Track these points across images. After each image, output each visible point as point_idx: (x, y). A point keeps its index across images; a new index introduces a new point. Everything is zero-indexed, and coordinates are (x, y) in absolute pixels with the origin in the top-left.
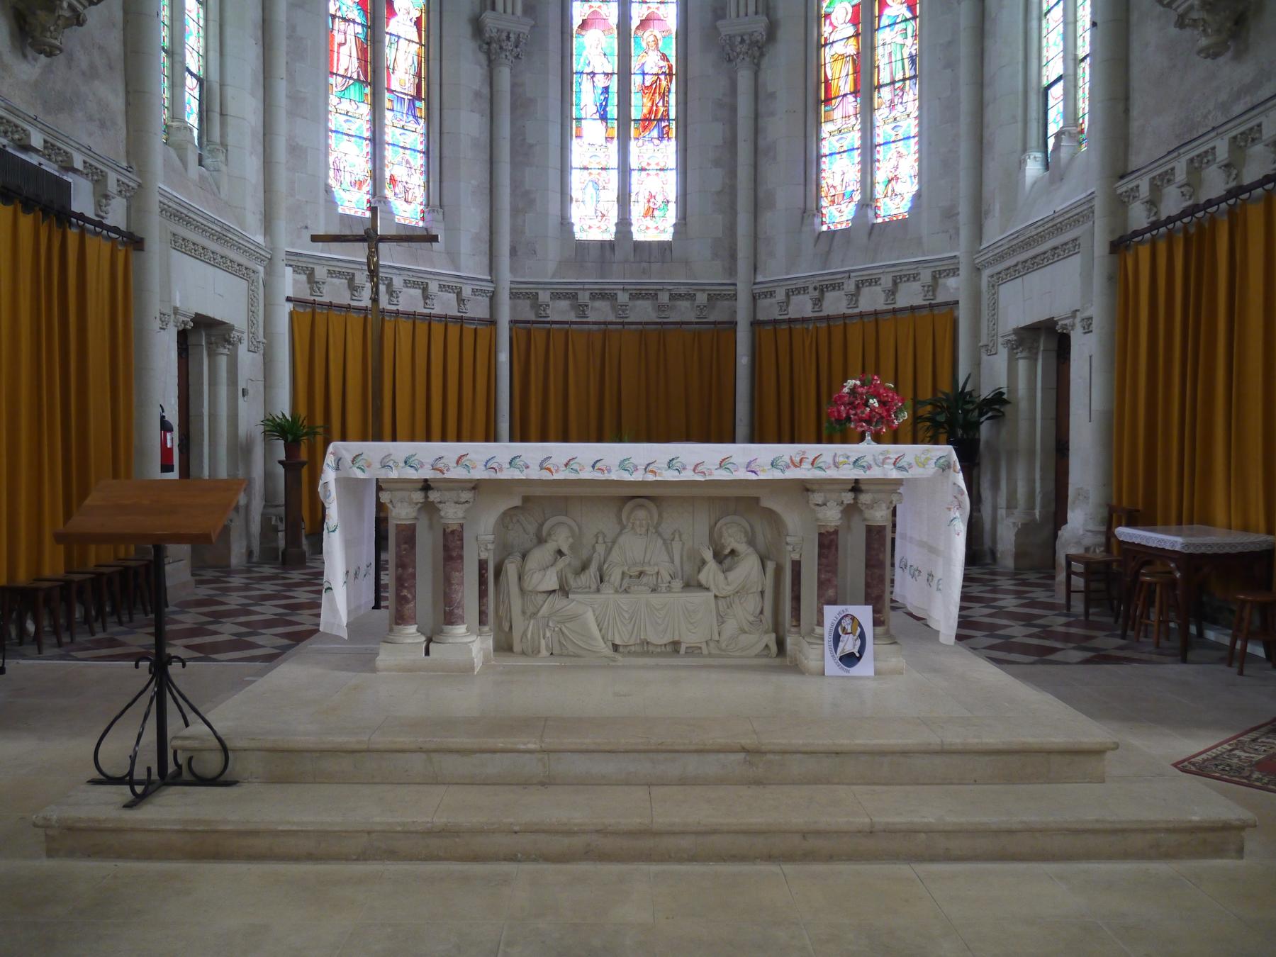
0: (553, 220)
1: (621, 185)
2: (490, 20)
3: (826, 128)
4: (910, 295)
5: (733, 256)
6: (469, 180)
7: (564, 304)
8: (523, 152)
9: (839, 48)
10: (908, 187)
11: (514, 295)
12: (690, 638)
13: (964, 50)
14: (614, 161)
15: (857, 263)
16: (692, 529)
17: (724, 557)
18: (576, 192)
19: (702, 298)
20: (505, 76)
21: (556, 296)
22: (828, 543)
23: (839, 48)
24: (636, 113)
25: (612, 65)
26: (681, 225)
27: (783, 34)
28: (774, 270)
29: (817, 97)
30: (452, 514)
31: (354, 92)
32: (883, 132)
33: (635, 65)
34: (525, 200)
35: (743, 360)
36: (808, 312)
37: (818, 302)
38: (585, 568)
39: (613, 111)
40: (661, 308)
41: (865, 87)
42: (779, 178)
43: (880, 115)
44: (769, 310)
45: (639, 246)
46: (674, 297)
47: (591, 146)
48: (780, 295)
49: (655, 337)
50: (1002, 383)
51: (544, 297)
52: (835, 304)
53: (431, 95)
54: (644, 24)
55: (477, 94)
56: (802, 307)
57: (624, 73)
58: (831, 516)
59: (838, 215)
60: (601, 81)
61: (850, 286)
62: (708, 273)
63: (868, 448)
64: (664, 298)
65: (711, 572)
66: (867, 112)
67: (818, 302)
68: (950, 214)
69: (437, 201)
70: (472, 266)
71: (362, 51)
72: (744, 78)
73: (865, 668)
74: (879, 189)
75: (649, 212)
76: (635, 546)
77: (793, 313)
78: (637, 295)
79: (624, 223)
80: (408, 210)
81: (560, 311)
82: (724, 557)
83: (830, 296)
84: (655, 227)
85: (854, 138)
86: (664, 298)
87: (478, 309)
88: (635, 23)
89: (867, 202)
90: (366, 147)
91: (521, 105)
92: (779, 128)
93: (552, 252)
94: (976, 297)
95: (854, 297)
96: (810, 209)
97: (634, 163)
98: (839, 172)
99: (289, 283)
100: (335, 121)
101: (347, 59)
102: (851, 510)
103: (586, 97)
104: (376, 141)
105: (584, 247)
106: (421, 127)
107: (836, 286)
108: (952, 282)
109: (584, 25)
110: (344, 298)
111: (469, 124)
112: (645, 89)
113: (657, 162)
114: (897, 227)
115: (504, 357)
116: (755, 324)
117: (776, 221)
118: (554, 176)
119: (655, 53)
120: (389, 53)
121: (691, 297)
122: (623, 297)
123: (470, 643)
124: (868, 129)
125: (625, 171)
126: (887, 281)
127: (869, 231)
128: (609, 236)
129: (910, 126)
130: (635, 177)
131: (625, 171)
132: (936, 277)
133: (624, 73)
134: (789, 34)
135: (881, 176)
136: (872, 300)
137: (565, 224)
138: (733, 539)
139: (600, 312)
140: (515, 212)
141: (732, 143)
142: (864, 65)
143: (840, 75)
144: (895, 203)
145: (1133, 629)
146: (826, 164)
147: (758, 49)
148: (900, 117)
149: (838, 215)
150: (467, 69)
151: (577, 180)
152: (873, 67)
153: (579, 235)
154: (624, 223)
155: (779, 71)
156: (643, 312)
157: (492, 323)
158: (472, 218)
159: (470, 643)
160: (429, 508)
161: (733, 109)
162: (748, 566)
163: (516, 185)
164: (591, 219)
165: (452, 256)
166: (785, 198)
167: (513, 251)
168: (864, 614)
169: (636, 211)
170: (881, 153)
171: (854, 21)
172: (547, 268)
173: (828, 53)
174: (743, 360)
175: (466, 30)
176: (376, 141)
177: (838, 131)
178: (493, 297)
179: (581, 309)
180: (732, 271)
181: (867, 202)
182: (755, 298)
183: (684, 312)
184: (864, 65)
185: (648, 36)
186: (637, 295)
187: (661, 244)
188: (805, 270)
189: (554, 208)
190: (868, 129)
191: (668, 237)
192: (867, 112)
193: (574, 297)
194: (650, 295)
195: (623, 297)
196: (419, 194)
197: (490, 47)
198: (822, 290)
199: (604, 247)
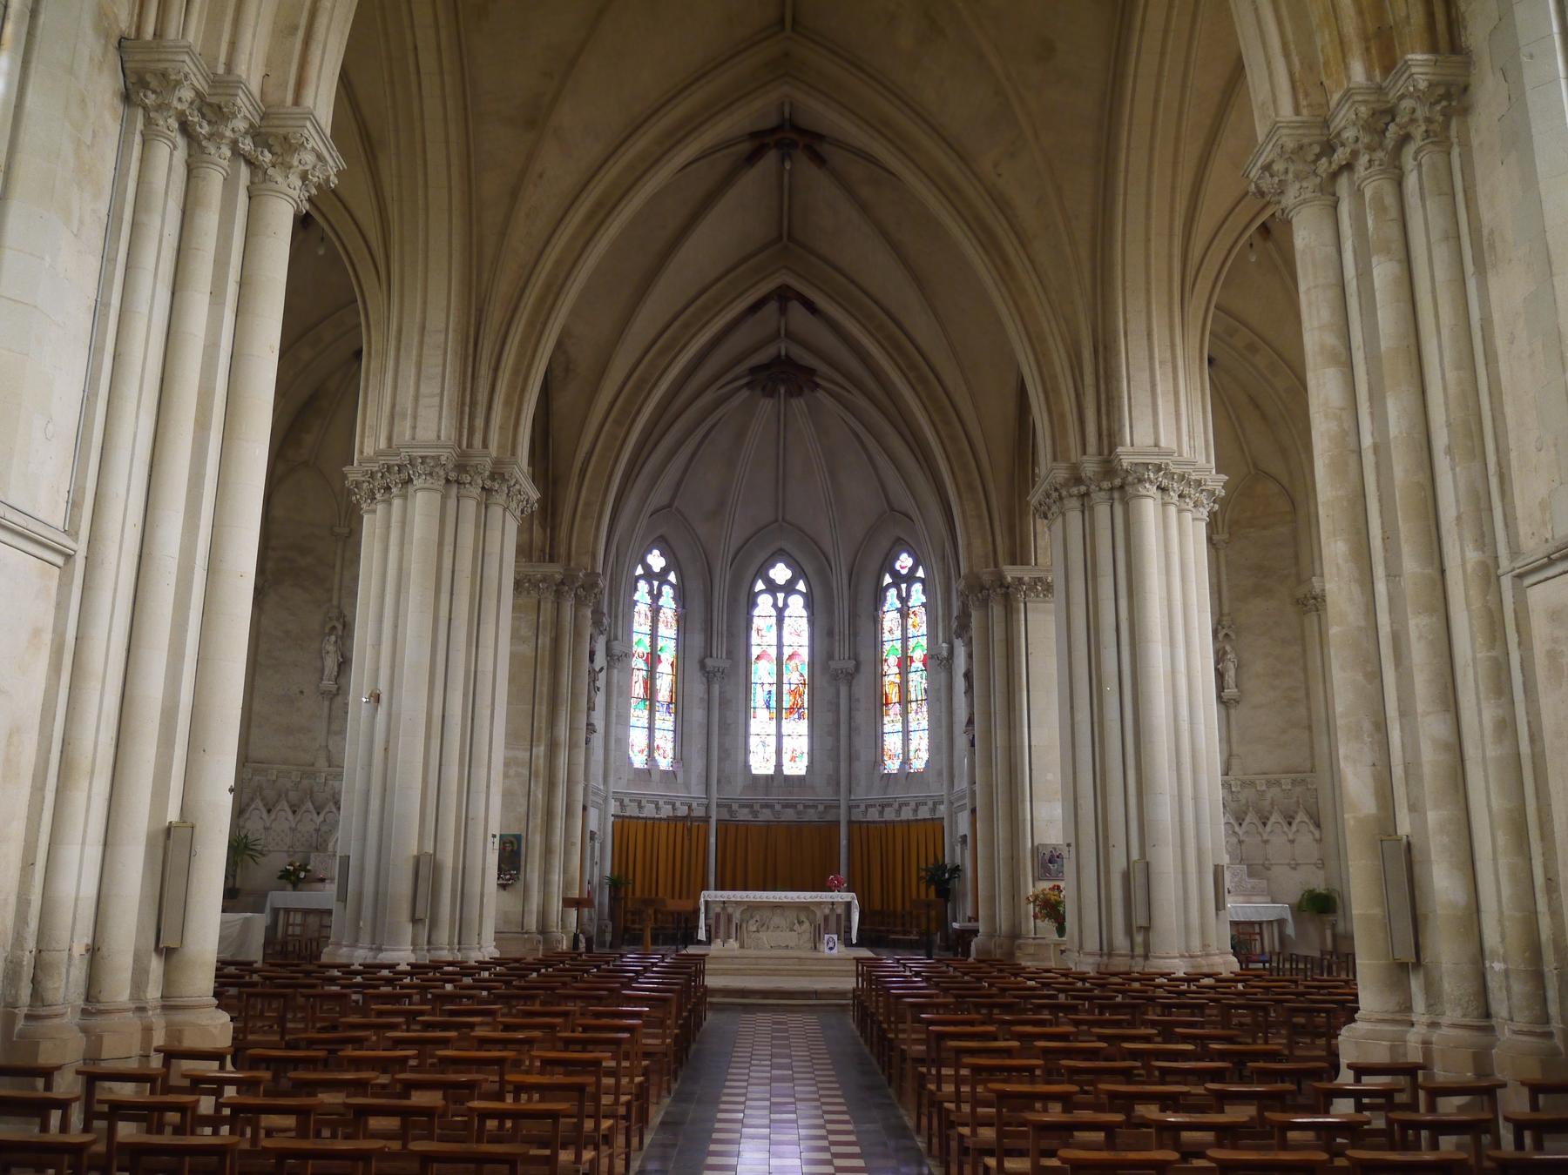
0: (741, 764)
1: (778, 744)
2: (709, 662)
3: (886, 719)
4: (924, 813)
5: (838, 784)
6: (697, 744)
7: (746, 810)
8: (725, 728)
9: (891, 678)
10: (925, 756)
11: (718, 806)
12: (791, 944)
13: (943, 694)
14: (774, 731)
15: (897, 793)
16: (792, 915)
17: (801, 923)
18: (752, 747)
19: (821, 808)
20: (716, 689)
21: (741, 806)
22: (826, 918)
23: (891, 678)
24: (785, 705)
25: (774, 679)
26: (810, 768)
27: (863, 669)
28: (860, 794)
29: (881, 703)
30: (730, 910)
31: (641, 705)
32: (913, 726)
33: (785, 680)
34: (725, 753)
35: (844, 842)
36: (877, 818)
37: (881, 813)
38: (763, 925)
39: (773, 704)
40: (799, 813)
41: (904, 701)
42: (861, 743)
43: (912, 716)
44: (857, 815)
45: (787, 777)
46: (806, 807)
47: (761, 724)
48: (863, 808)
49: (796, 830)
50: (958, 861)
51: (735, 807)
52: (890, 815)
53: (678, 702)
54: (791, 657)
55: (702, 699)
56: (873, 815)
57: (780, 684)
58: (827, 911)
59: (892, 766)
60: (767, 688)
61: (896, 806)
62: (824, 793)
63: (836, 893)
64: (800, 807)
65: (797, 927)
66: (905, 714)
67: (881, 813)
68: (940, 774)
69: (680, 756)
70: (697, 791)
71: (645, 683)
72: (844, 690)
73: (835, 951)
74: (912, 754)
75: (793, 759)
76: (777, 920)
77: (869, 818)
78: (785, 806)
79: (779, 765)
80: (664, 763)
81: (743, 815)
82: (801, 923)
83: (887, 810)
84: (796, 767)
85: (899, 727)
86: (800, 807)
87: (699, 812)
88: (785, 657)
89: (906, 761)
90: (646, 732)
91: (724, 703)
92: (861, 717)
93: (740, 782)
94: (951, 816)
95: (898, 811)
96: (878, 761)
97: (785, 731)
98: (893, 742)
99: (613, 807)
100: (633, 721)
101: (638, 689)
102: (832, 910)
103: (759, 696)
104: (651, 728)
105: (757, 778)
106: (672, 718)
107: (890, 805)
108: (942, 808)
109: (758, 658)
110: (636, 813)
111: (697, 715)
112: (791, 692)
113: (798, 733)
114: (918, 775)
115: (713, 840)
116: (850, 823)
117: (861, 767)
118: (741, 740)
119: (797, 673)
120: (658, 682)
121: (815, 807)
122: (778, 807)
123: (733, 944)
124: (905, 722)
125: (779, 736)
126: (913, 805)
127: (906, 776)
128: (771, 771)
129: (925, 724)
130: (785, 740)
131: (779, 736)
132: (935, 804)
133: (780, 684)
134: (866, 669)
135: (912, 748)
136: (907, 814)
137: (747, 766)
138: (803, 918)
139: (766, 815)
140: (720, 760)
141: (837, 724)
142: (903, 687)
143: (893, 693)
144: (919, 763)
145: (839, 916)
146: (887, 737)
147: (850, 676)
148: (920, 720)
149: (892, 766)
150: (697, 688)
151: (754, 742)
152: (908, 691)
153: (754, 772)
154: (779, 765)
155: (863, 680)
156: (789, 815)
157: (706, 819)
158: (697, 765)
159: (733, 944)
160: (724, 909)
161: (838, 705)
162: (806, 925)
163: (721, 745)
164: (761, 763)
165: (687, 786)
166: (865, 755)
167: (719, 781)
168: (835, 937)
169: (786, 758)
170: (913, 736)
171: (899, 665)
172: (736, 791)
173: (886, 679)
174: (844, 842)
175: (696, 666)
176: (651, 728)
177: (892, 723)
178: (707, 807)
179: (755, 813)
180: (837, 792)
181: (906, 761)
182: (850, 808)
183: (812, 815)
184: (903, 687)
185: (793, 663)
186: (785, 806)
187: (799, 777)
188: (875, 795)
189: (741, 758)
190: (905, 722)
191: (803, 772)
192: (905, 714)
193: (751, 806)
194: (794, 806)
195: (778, 807)
196: (670, 754)
197: (709, 675)
198: (883, 806)
199: (768, 779)
